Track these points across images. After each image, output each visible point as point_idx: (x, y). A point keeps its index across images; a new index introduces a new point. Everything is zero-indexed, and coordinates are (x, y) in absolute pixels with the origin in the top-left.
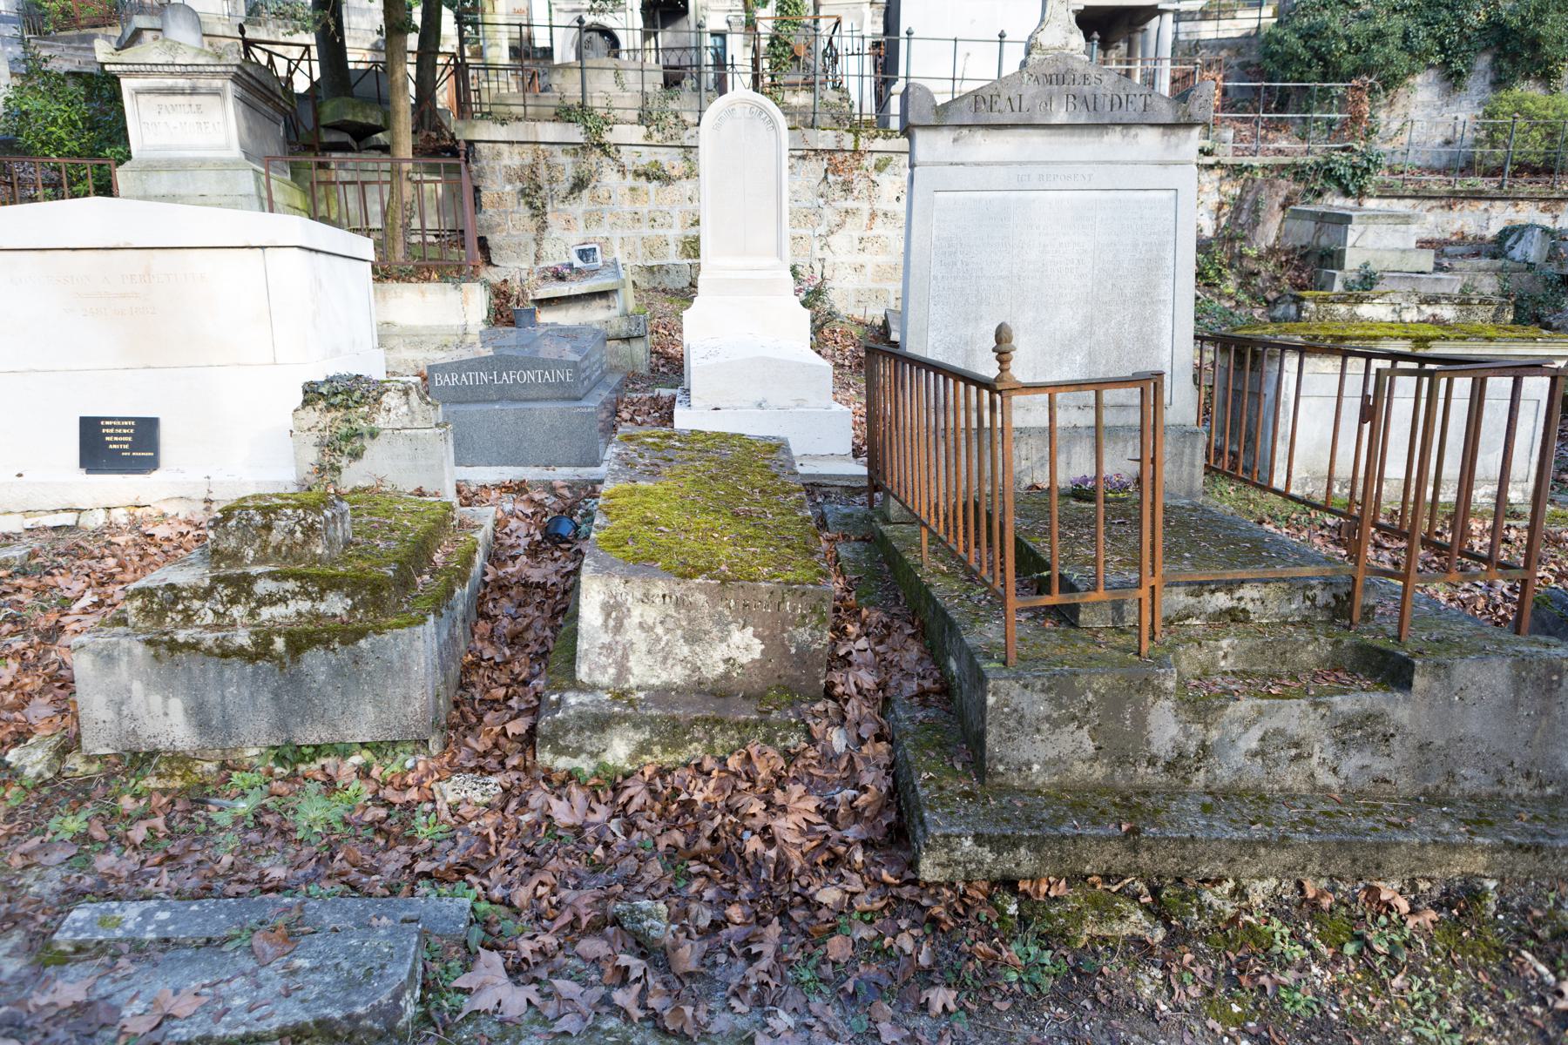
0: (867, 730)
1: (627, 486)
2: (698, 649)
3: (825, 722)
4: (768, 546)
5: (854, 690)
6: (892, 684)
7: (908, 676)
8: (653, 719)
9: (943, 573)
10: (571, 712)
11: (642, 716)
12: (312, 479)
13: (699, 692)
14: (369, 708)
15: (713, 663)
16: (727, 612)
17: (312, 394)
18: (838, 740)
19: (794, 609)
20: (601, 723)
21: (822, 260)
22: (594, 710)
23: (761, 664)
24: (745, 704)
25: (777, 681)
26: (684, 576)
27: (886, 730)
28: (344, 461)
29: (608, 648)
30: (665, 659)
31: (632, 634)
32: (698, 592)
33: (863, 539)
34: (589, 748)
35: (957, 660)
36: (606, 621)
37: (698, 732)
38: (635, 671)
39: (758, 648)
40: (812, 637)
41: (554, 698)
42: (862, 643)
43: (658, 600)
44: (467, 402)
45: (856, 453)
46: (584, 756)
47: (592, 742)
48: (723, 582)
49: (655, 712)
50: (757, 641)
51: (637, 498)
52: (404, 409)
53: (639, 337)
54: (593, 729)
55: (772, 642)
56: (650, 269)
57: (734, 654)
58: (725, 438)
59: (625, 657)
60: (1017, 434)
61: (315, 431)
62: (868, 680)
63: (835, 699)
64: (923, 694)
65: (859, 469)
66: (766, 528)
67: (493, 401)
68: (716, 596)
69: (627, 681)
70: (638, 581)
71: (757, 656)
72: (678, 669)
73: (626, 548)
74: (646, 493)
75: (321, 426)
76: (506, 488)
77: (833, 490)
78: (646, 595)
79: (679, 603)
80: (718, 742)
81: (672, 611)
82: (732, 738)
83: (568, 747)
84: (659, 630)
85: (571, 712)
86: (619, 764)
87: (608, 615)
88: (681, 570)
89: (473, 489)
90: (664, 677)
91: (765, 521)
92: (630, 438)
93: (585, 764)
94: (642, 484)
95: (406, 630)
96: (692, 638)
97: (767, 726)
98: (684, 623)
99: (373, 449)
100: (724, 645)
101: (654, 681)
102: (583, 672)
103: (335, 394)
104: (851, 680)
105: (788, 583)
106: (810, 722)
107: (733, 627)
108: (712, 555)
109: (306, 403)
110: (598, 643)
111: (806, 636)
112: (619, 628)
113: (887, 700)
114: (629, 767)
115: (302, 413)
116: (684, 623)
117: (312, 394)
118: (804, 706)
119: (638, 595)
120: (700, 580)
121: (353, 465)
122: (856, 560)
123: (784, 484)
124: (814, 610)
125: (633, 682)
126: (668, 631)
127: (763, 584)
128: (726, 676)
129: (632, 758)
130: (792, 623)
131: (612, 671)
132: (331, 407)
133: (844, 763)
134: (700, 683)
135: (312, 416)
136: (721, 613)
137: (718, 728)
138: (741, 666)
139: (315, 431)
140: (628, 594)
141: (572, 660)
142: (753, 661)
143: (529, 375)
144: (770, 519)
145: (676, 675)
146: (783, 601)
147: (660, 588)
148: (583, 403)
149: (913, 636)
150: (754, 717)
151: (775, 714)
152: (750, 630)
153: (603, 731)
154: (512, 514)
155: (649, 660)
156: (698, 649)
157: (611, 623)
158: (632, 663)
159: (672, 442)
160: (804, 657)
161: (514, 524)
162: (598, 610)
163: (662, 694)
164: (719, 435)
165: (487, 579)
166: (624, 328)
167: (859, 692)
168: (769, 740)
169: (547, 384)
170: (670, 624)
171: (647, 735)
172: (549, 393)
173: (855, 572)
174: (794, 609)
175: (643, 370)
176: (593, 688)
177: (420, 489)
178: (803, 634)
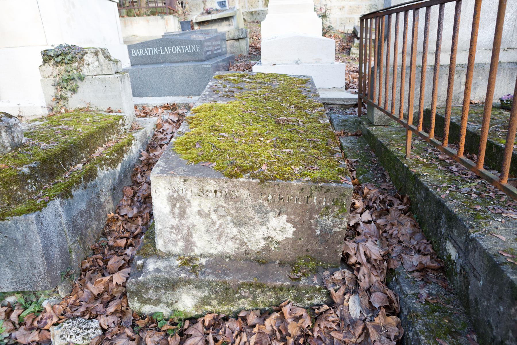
0: (377, 300)
1: (209, 105)
2: (244, 230)
3: (343, 289)
4: (300, 147)
5: (364, 260)
6: (394, 255)
7: (407, 249)
8: (209, 283)
9: (424, 164)
10: (149, 277)
11: (202, 281)
12: (54, 104)
13: (246, 260)
14: (7, 270)
15: (256, 239)
16: (266, 204)
17: (47, 57)
18: (354, 307)
19: (320, 202)
20: (172, 285)
21: (326, 5)
22: (165, 275)
23: (293, 241)
24: (281, 271)
25: (305, 253)
26: (231, 176)
27: (395, 305)
28: (69, 94)
29: (177, 229)
30: (220, 237)
31: (193, 218)
32: (243, 188)
33: (356, 135)
34: (165, 300)
35: (456, 245)
36: (172, 209)
37: (244, 292)
38: (198, 244)
39: (290, 231)
40: (336, 223)
41: (139, 262)
42: (367, 216)
43: (212, 195)
44: (148, 64)
45: (347, 87)
46: (162, 305)
47: (167, 296)
48: (262, 181)
49: (211, 278)
50: (290, 225)
51: (213, 112)
52: (97, 63)
53: (243, 38)
54: (166, 288)
55: (303, 227)
56: (251, 13)
57: (272, 234)
58: (276, 76)
59: (189, 234)
60: (459, 68)
61: (52, 77)
62: (375, 251)
63: (351, 267)
64: (423, 270)
65: (352, 96)
66: (298, 132)
67: (161, 63)
68: (256, 192)
69: (193, 251)
70: (194, 180)
71: (290, 235)
72: (230, 243)
73: (193, 151)
74: (220, 109)
75: (54, 74)
76: (166, 107)
77: (335, 106)
78: (201, 190)
79: (228, 197)
80: (260, 299)
81: (222, 203)
82: (271, 297)
83: (150, 299)
84: (214, 216)
85: (149, 277)
86: (188, 310)
87: (174, 205)
88: (229, 170)
89: (151, 108)
90: (220, 248)
91: (298, 128)
92: (220, 77)
93: (164, 310)
94: (220, 103)
95: (22, 217)
96: (239, 223)
97: (297, 289)
98: (233, 212)
99: (84, 87)
100: (264, 228)
101: (215, 252)
102: (160, 244)
103: (58, 56)
104: (362, 250)
105: (315, 181)
106: (331, 290)
107: (271, 215)
108: (257, 156)
109: (45, 62)
110: (169, 225)
111: (329, 222)
112: (183, 214)
113: (391, 272)
114: (195, 313)
115: (43, 67)
116: (233, 212)
117: (47, 57)
118: (326, 273)
119: (196, 190)
120: (243, 180)
121: (73, 96)
122: (353, 148)
123: (310, 102)
124: (336, 203)
125: (197, 251)
126: (220, 217)
127: (295, 183)
128: (267, 249)
129: (197, 307)
130: (318, 212)
131: (181, 244)
132: (57, 63)
133: (359, 331)
134: (247, 254)
135: (49, 68)
136: (261, 205)
137: (259, 291)
138: (278, 243)
139: (52, 77)
140: (189, 189)
141: (152, 238)
142: (287, 239)
143: (178, 49)
144: (301, 126)
145: (229, 248)
146: (311, 195)
147: (211, 185)
148: (206, 63)
149: (404, 212)
150: (287, 283)
151: (303, 281)
152: (284, 217)
153: (174, 290)
154: (167, 121)
155: (208, 237)
156: (244, 230)
157: (177, 211)
158: (195, 238)
159: (245, 79)
160: (326, 237)
161: (166, 126)
162: (166, 201)
163: (219, 263)
164: (272, 75)
165: (142, 159)
166: (236, 34)
167: (369, 260)
168: (298, 299)
169: (187, 53)
170: (221, 211)
171: (207, 293)
172: (188, 58)
173: (354, 157)
174: (320, 202)
175: (245, 54)
176: (168, 255)
177: (109, 108)
178: (327, 221)
